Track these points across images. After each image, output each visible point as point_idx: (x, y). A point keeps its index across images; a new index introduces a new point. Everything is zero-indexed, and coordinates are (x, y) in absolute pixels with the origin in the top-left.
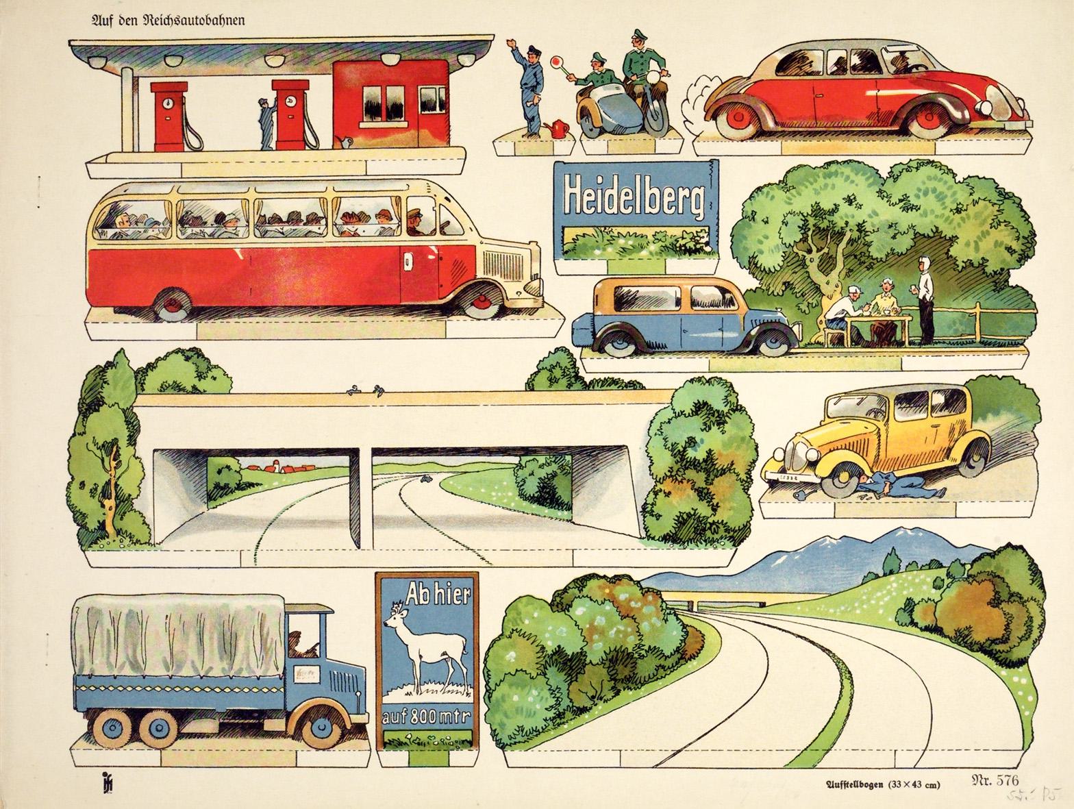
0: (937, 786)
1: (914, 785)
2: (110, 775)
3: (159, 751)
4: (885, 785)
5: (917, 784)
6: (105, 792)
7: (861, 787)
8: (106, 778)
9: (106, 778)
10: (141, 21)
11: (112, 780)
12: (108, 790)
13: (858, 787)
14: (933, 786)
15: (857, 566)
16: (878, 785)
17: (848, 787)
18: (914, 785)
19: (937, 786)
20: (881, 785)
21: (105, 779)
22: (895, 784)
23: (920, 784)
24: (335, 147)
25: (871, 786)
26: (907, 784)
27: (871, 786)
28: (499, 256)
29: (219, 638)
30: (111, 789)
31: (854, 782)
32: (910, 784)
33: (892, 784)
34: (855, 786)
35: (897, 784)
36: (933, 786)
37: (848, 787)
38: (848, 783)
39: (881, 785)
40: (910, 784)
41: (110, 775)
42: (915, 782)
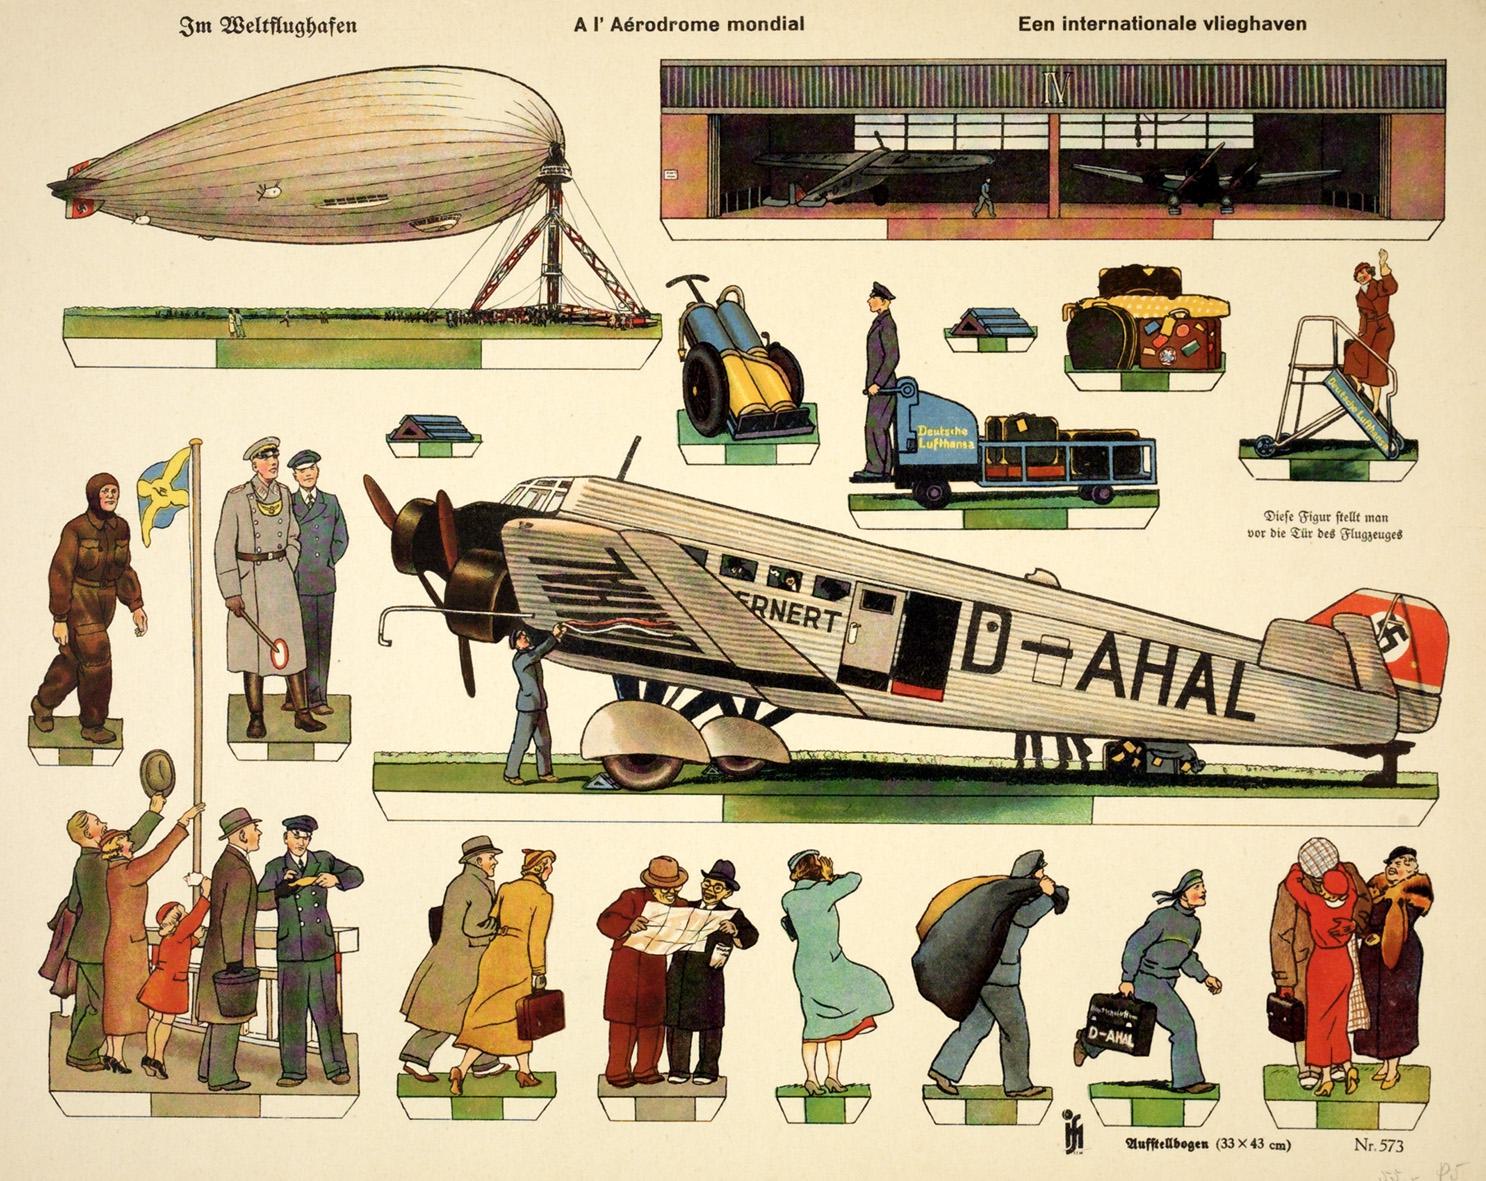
0: (1287, 1147)
1: (1254, 1145)
2: (1079, 1117)
3: (964, 1101)
4: (1212, 1145)
5: (1258, 1143)
6: (1068, 1152)
7: (1192, 1142)
8: (1070, 1121)
9: (1070, 1121)
10: (217, 27)
11: (1081, 1127)
12: (1074, 1148)
13: (1171, 1147)
14: (1280, 1146)
15: (1322, 845)
16: (1201, 1145)
17: (1157, 1147)
18: (1254, 1145)
19: (1287, 1147)
20: (1205, 1145)
21: (1068, 1125)
22: (1225, 1143)
23: (1261, 1143)
24: (726, 818)
25: (1191, 1146)
26: (1242, 1144)
27: (1191, 1146)
28: (698, 68)
29: (996, 724)
30: (1081, 1146)
31: (1167, 1140)
32: (1248, 1144)
33: (1221, 1143)
34: (1167, 1147)
35: (1228, 1143)
36: (1280, 1146)
37: (1157, 1147)
38: (1157, 1142)
39: (1205, 1145)
40: (1248, 1144)
41: (1079, 1117)
42: (1255, 1141)
